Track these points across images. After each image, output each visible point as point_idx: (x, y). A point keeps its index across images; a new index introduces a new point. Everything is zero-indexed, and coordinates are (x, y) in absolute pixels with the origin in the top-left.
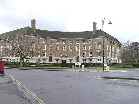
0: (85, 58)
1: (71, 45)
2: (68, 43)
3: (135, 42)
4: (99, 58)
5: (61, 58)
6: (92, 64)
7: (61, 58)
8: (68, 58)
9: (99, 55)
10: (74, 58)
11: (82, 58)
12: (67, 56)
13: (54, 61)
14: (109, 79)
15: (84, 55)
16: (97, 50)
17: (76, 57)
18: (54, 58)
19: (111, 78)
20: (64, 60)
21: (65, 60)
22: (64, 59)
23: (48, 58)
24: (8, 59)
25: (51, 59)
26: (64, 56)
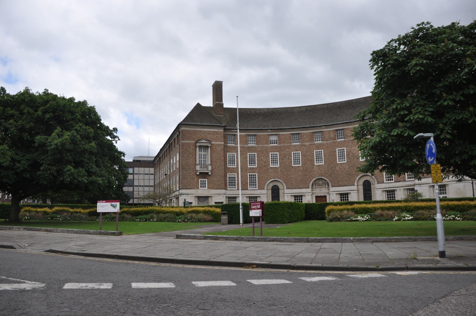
0: (390, 185)
1: (341, 144)
2: (331, 139)
3: (403, 34)
4: (203, 192)
5: (309, 190)
6: (59, 218)
7: (309, 190)
8: (332, 189)
9: (203, 185)
10: (355, 188)
11: (383, 186)
12: (330, 184)
13: (287, 196)
14: (308, 272)
15: (253, 183)
16: (198, 168)
17: (361, 182)
18: (286, 191)
19: (258, 266)
20: (319, 195)
21: (323, 195)
22: (321, 191)
23: (264, 191)
24: (394, 191)
25: (275, 192)
26: (320, 182)
